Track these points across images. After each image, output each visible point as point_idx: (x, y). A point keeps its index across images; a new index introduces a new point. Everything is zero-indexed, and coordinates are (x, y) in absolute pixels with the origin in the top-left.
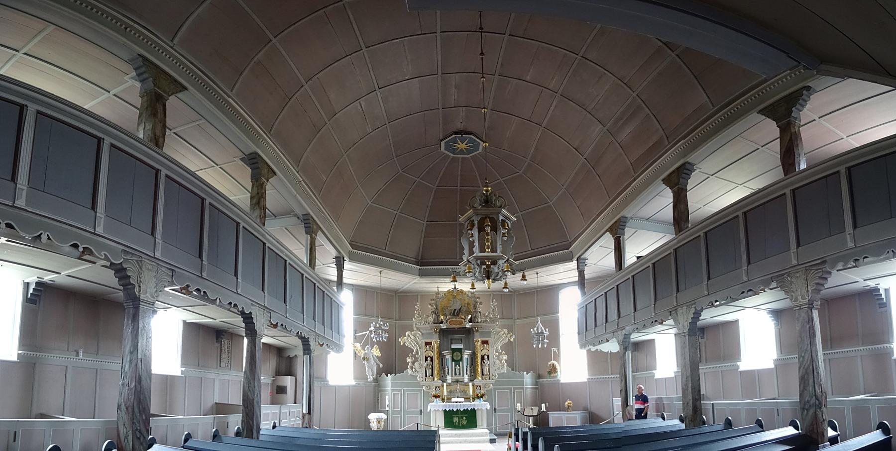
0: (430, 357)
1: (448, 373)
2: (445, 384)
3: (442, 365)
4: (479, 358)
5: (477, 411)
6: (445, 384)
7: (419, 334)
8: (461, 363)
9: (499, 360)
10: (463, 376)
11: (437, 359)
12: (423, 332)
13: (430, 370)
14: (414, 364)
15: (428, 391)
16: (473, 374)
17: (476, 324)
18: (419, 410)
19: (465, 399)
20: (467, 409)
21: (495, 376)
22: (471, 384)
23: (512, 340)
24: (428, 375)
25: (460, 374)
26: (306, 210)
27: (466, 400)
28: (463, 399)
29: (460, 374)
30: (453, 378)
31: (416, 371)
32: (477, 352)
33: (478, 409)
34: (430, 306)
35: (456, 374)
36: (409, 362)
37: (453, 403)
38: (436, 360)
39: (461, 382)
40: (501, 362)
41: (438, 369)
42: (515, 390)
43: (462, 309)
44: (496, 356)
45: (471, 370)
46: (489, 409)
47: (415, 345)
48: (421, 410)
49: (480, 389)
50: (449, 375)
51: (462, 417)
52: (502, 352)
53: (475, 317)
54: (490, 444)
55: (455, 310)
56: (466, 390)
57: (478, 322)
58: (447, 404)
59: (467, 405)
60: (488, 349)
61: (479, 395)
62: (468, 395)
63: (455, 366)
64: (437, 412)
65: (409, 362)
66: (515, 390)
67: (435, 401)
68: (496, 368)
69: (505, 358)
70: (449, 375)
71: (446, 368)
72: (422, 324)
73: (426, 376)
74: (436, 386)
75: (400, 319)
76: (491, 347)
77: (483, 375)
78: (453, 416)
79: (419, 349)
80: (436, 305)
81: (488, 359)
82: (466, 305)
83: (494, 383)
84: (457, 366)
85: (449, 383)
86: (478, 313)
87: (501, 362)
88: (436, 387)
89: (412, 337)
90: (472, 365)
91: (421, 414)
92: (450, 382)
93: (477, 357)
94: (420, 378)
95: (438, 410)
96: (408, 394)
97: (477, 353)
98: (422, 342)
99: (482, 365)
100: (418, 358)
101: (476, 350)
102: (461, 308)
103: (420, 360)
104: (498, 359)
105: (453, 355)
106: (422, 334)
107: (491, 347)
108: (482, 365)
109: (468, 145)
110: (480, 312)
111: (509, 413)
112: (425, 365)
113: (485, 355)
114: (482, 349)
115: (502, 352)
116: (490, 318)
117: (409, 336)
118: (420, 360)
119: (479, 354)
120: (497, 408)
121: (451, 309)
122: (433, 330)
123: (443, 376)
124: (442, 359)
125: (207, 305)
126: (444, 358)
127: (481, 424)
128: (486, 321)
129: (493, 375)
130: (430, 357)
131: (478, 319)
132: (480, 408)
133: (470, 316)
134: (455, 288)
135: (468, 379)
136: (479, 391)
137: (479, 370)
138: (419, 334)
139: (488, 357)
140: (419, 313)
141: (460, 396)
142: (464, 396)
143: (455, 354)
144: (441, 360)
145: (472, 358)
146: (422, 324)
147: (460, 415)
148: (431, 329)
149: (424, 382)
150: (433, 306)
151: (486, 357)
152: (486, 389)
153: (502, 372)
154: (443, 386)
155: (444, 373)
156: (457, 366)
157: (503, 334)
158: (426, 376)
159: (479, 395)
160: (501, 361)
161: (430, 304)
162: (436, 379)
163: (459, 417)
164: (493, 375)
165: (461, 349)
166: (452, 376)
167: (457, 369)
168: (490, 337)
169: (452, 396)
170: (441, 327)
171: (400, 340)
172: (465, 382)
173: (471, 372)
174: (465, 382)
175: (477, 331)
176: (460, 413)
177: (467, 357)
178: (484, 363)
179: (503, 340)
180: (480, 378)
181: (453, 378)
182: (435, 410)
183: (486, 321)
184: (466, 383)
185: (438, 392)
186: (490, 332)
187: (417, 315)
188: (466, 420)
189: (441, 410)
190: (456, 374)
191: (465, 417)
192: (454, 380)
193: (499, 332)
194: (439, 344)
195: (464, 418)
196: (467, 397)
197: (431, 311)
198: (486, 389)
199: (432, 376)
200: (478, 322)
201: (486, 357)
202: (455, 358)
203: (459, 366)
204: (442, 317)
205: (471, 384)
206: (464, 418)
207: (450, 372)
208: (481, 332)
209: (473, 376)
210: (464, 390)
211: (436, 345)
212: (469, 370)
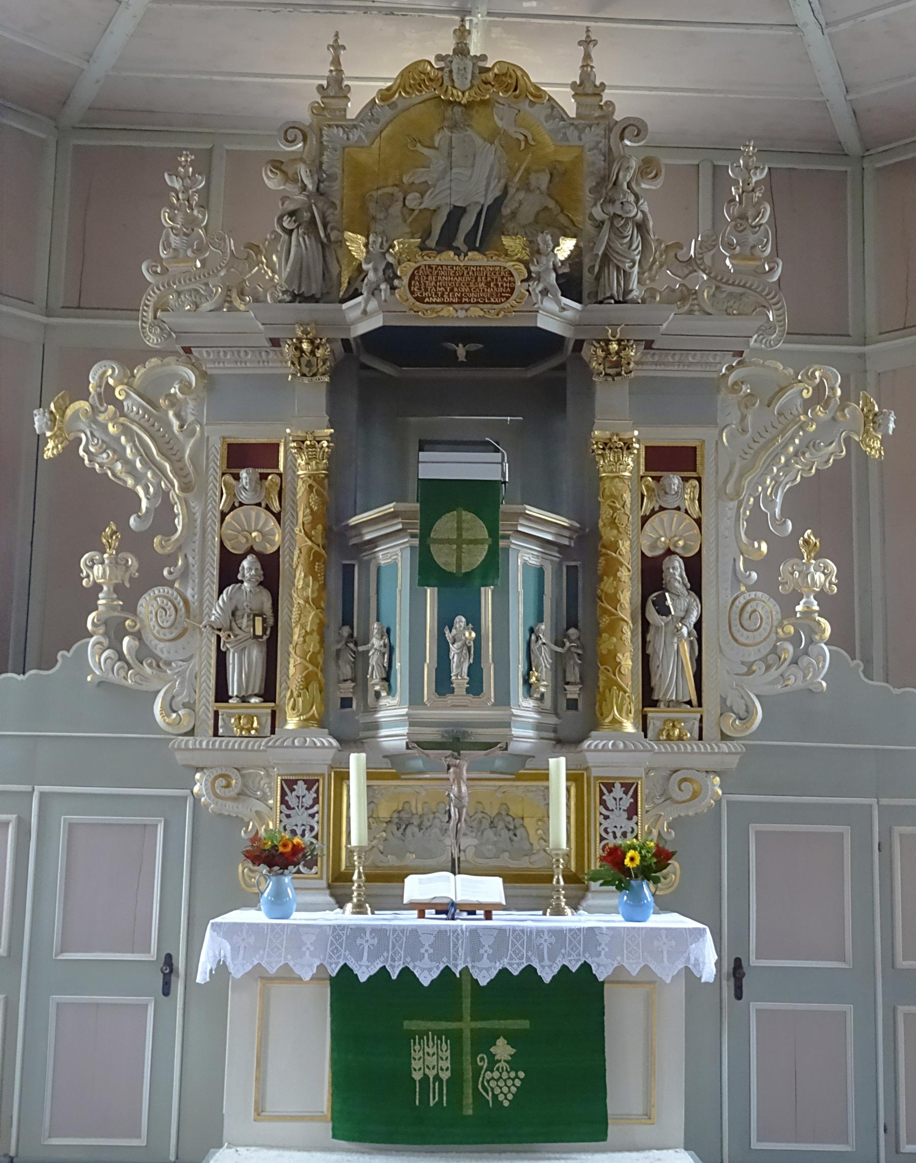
0: (261, 557)
1: (387, 679)
2: (356, 762)
3: (347, 620)
4: (624, 574)
5: (609, 992)
6: (356, 762)
7: (186, 387)
8: (487, 595)
9: (774, 595)
10: (504, 699)
11: (310, 571)
12: (210, 368)
13: (256, 654)
14: (131, 607)
15: (230, 808)
16: (573, 692)
17: (611, 308)
18: (152, 955)
19: (510, 879)
20: (530, 970)
21: (746, 717)
22: (558, 766)
23: (875, 447)
24: (233, 689)
25: (475, 686)
26: (661, 717)
27: (523, 889)
28: (497, 883)
29: (475, 686)
30: (422, 713)
31: (143, 653)
32: (613, 523)
33: (620, 977)
34: (272, 182)
35: (443, 684)
36: (97, 588)
37: (409, 918)
38: (300, 574)
39: (488, 746)
40: (788, 611)
41: (313, 645)
42: (898, 830)
43: (506, 211)
44: (750, 565)
45: (559, 662)
46: (708, 973)
47: (148, 460)
48: (169, 960)
49: (632, 811)
50: (390, 691)
51: (483, 1042)
52: (798, 531)
53: (606, 259)
54: (683, 1150)
55: (457, 213)
56: (515, 810)
57: (623, 299)
58: (369, 919)
59: (531, 936)
60: (695, 511)
61: (632, 860)
62: (530, 853)
63: (445, 621)
64: (279, 991)
65: (97, 588)
66: (898, 830)
67: (268, 889)
68: (752, 655)
69: (819, 577)
70: (390, 691)
71: (376, 642)
72: (206, 306)
73: (222, 694)
74: (292, 772)
75: (78, 307)
76: (721, 494)
77: (649, 699)
78: (408, 1025)
79: (176, 492)
80: (317, 168)
81: (696, 586)
82: (543, 180)
83: (733, 762)
84: (460, 621)
85: (393, 758)
86: (630, 229)
87: (788, 611)
88: (290, 784)
89: (133, 404)
90: (572, 623)
91: (166, 991)
92: (401, 743)
93: (613, 567)
94: (169, 708)
95: (287, 976)
96: (71, 827)
97: (608, 534)
98: (204, 441)
99: (646, 625)
100: (171, 559)
101: (605, 513)
102: (499, 202)
103: (185, 574)
104: (769, 584)
105: (424, 536)
106: (208, 380)
107: (721, 494)
108: (646, 625)
109: (603, 788)
110: (641, 227)
111: (849, 1008)
112: (216, 612)
113: (669, 552)
114: (647, 506)
115: (798, 531)
116: (719, 278)
117: (107, 395)
118: (185, 574)
119: (625, 546)
120: (754, 961)
121: (427, 203)
122: (287, 349)
123: (346, 703)
124: (348, 571)
125: (661, 675)
126: (366, 566)
127: (637, 1108)
128: (687, 295)
129: (725, 709)
130: (261, 557)
131: (627, 275)
132: (634, 970)
133: (566, 247)
134: (461, 50)
135: (539, 727)
136: (619, 820)
137: (628, 662)
138: (186, 387)
139: (693, 567)
140: (191, 223)
141: (469, 856)
142: (506, 861)
143: (445, 526)
144: (335, 584)
145: (572, 571)
146: (206, 306)
147: (467, 1025)
148: (275, 343)
149: (205, 740)
150: (295, 179)
151: (676, 570)
152: (670, 814)
153: (794, 681)
154: (343, 777)
155: (359, 678)
156: (460, 621)
157: (808, 404)
158: (222, 694)
159: (632, 860)
160: (788, 602)
161: (277, 165)
162: (292, 723)
163: (455, 1039)
164: (725, 709)
165: (491, 484)
166: (415, 699)
167: (454, 649)
168: (712, 421)
169: (411, 859)
170: (347, 326)
171: (39, 421)
172: (516, 747)
173: (560, 680)
174: (516, 747)
175: (616, 367)
176: (467, 1003)
177: (534, 562)
178: (664, 611)
179: (810, 444)
180: (629, 727)
181: (422, 713)
182: (259, 974)
183: (687, 295)
184: (523, 758)
185: (300, 818)
186: (713, 386)
187: (174, 240)
188: (514, 1064)
189: (307, 977)
190: (443, 684)
191: (512, 1038)
192: (430, 734)
193: (782, 390)
194: (333, 457)
195: (503, 1050)
196: (523, 864)
197: (280, 208)
198: (670, 814)
199: (269, 693)
200: (623, 299)
201: (676, 570)
202: (444, 558)
203: (475, 622)
204: (356, 244)
205: (558, 766)
206: (503, 1050)
207: (400, 665)
208: (642, 386)
209: (572, 704)
210: (504, 812)
211: (303, 467)
212: (544, 659)
